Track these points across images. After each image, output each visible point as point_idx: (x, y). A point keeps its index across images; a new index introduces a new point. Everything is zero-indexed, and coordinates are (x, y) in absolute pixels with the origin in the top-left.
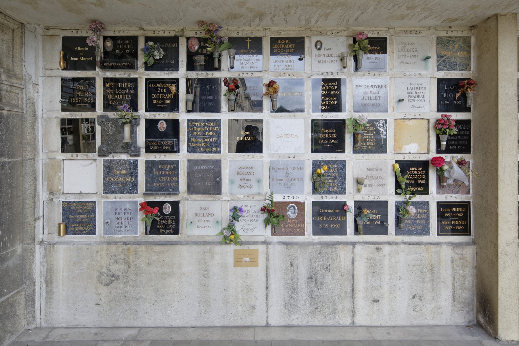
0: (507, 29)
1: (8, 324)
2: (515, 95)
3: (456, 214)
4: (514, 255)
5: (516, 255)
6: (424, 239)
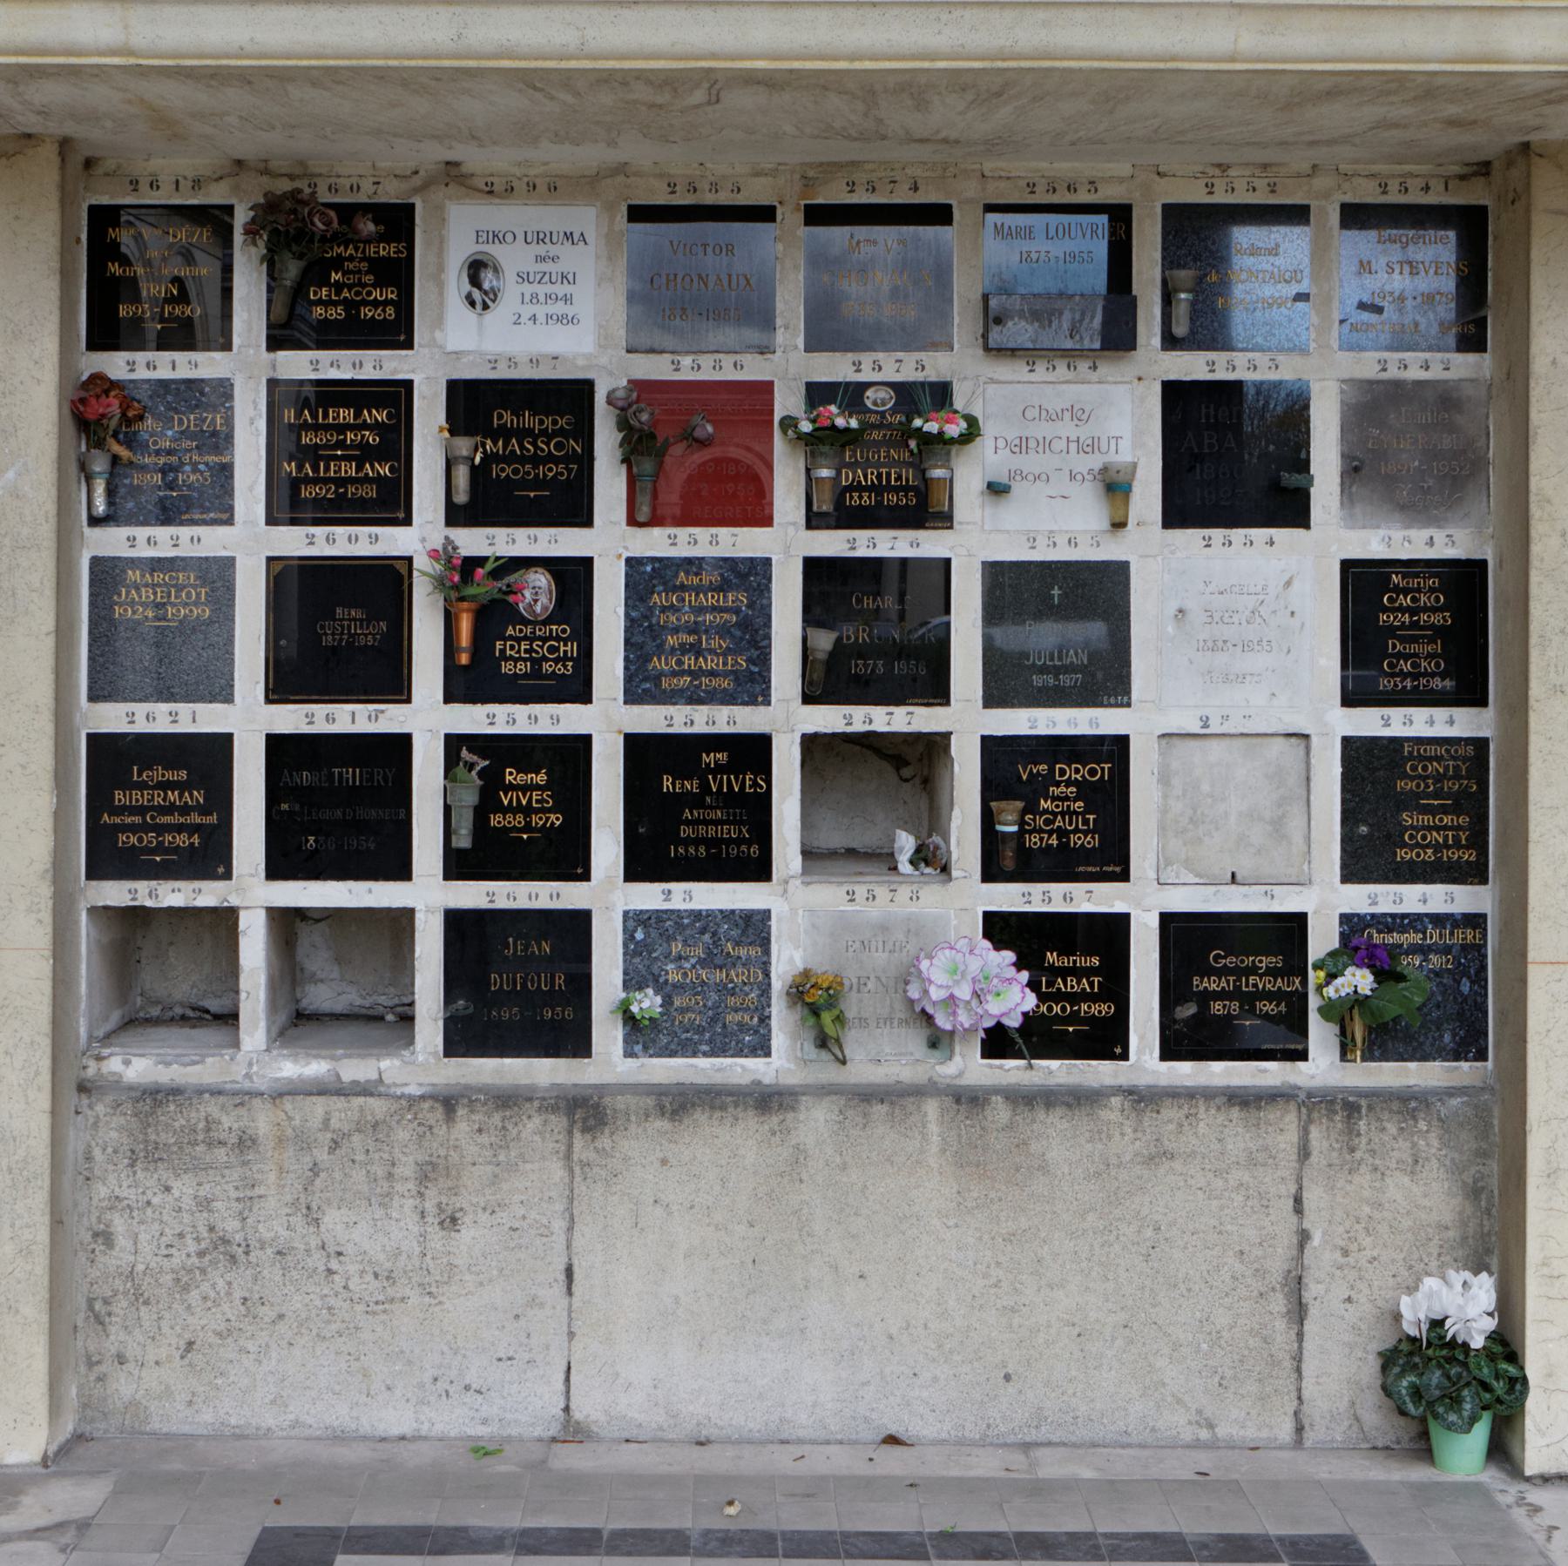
6: (1097, 1072)
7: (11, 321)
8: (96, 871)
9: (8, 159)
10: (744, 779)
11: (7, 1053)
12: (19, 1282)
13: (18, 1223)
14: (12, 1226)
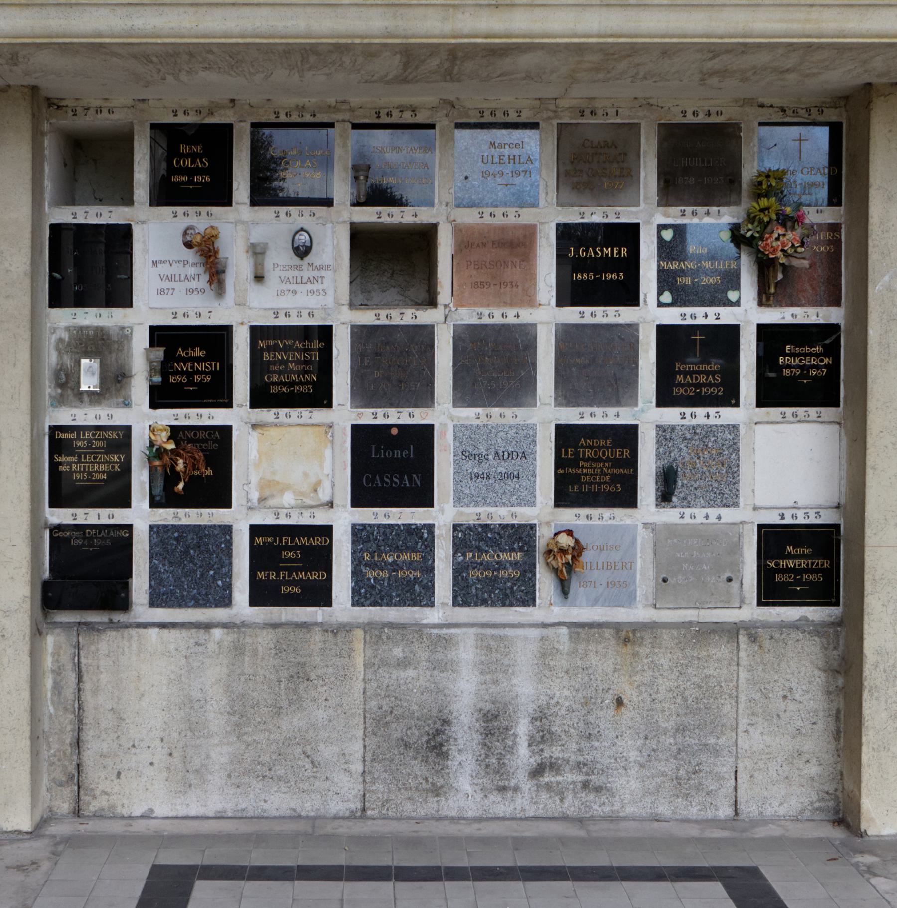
0: (8, 123)
1: (770, 809)
2: (25, 274)
3: (805, 577)
4: (22, 637)
5: (24, 639)
6: (219, 614)
7: (887, 190)
8: (55, 502)
9: (885, 96)
10: (616, 451)
11: (883, 605)
12: (890, 734)
13: (889, 701)
14: (886, 702)
